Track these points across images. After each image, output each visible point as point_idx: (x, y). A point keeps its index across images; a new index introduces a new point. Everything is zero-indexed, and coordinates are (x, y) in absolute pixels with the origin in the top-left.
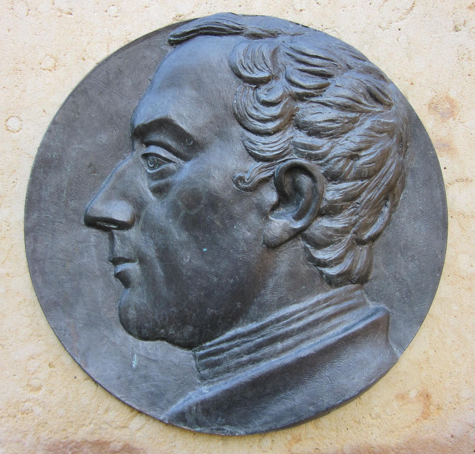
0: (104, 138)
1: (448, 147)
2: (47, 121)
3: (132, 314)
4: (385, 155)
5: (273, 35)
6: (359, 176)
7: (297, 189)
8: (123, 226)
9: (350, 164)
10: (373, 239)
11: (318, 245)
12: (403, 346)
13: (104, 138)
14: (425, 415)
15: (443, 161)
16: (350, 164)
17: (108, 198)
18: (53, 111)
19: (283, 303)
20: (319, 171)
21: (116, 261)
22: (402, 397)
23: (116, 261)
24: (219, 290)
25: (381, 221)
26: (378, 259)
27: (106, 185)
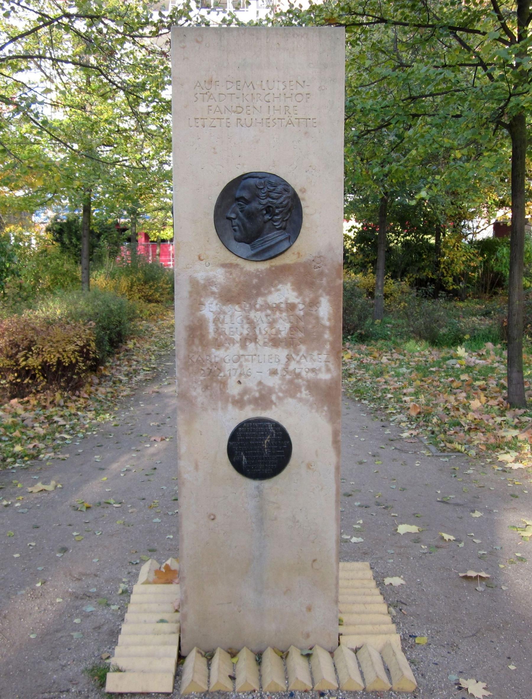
0: (229, 200)
1: (304, 199)
2: (217, 197)
3: (237, 237)
4: (288, 203)
5: (264, 178)
6: (282, 207)
7: (270, 211)
8: (234, 219)
9: (384, 627)
10: (287, 220)
11: (275, 222)
12: (294, 242)
13: (229, 200)
14: (299, 257)
15: (302, 203)
16: (384, 627)
17: (231, 213)
18: (218, 195)
19: (268, 234)
20: (274, 207)
21: (233, 226)
22: (294, 253)
23: (233, 226)
24: (386, 352)
25: (288, 216)
26: (288, 225)
27: (230, 211)
